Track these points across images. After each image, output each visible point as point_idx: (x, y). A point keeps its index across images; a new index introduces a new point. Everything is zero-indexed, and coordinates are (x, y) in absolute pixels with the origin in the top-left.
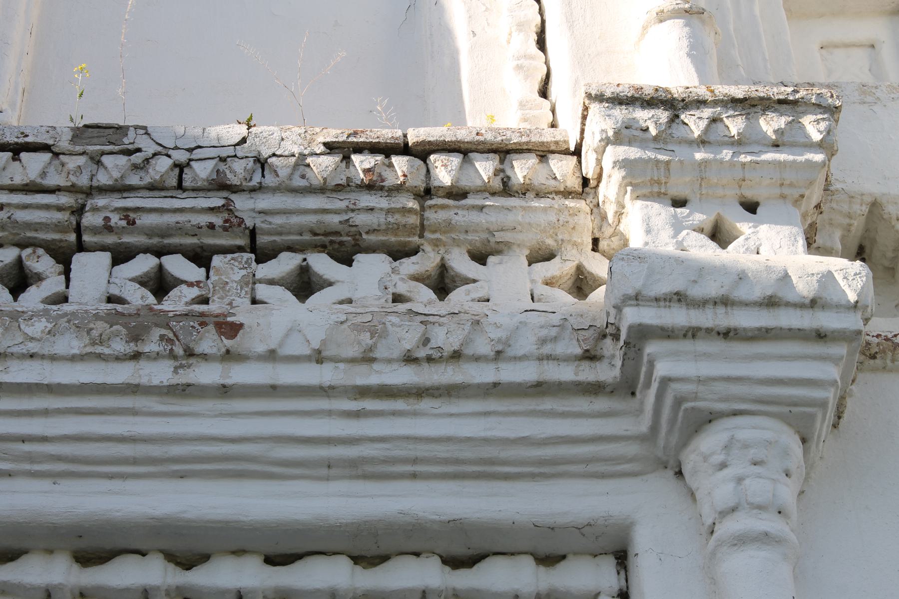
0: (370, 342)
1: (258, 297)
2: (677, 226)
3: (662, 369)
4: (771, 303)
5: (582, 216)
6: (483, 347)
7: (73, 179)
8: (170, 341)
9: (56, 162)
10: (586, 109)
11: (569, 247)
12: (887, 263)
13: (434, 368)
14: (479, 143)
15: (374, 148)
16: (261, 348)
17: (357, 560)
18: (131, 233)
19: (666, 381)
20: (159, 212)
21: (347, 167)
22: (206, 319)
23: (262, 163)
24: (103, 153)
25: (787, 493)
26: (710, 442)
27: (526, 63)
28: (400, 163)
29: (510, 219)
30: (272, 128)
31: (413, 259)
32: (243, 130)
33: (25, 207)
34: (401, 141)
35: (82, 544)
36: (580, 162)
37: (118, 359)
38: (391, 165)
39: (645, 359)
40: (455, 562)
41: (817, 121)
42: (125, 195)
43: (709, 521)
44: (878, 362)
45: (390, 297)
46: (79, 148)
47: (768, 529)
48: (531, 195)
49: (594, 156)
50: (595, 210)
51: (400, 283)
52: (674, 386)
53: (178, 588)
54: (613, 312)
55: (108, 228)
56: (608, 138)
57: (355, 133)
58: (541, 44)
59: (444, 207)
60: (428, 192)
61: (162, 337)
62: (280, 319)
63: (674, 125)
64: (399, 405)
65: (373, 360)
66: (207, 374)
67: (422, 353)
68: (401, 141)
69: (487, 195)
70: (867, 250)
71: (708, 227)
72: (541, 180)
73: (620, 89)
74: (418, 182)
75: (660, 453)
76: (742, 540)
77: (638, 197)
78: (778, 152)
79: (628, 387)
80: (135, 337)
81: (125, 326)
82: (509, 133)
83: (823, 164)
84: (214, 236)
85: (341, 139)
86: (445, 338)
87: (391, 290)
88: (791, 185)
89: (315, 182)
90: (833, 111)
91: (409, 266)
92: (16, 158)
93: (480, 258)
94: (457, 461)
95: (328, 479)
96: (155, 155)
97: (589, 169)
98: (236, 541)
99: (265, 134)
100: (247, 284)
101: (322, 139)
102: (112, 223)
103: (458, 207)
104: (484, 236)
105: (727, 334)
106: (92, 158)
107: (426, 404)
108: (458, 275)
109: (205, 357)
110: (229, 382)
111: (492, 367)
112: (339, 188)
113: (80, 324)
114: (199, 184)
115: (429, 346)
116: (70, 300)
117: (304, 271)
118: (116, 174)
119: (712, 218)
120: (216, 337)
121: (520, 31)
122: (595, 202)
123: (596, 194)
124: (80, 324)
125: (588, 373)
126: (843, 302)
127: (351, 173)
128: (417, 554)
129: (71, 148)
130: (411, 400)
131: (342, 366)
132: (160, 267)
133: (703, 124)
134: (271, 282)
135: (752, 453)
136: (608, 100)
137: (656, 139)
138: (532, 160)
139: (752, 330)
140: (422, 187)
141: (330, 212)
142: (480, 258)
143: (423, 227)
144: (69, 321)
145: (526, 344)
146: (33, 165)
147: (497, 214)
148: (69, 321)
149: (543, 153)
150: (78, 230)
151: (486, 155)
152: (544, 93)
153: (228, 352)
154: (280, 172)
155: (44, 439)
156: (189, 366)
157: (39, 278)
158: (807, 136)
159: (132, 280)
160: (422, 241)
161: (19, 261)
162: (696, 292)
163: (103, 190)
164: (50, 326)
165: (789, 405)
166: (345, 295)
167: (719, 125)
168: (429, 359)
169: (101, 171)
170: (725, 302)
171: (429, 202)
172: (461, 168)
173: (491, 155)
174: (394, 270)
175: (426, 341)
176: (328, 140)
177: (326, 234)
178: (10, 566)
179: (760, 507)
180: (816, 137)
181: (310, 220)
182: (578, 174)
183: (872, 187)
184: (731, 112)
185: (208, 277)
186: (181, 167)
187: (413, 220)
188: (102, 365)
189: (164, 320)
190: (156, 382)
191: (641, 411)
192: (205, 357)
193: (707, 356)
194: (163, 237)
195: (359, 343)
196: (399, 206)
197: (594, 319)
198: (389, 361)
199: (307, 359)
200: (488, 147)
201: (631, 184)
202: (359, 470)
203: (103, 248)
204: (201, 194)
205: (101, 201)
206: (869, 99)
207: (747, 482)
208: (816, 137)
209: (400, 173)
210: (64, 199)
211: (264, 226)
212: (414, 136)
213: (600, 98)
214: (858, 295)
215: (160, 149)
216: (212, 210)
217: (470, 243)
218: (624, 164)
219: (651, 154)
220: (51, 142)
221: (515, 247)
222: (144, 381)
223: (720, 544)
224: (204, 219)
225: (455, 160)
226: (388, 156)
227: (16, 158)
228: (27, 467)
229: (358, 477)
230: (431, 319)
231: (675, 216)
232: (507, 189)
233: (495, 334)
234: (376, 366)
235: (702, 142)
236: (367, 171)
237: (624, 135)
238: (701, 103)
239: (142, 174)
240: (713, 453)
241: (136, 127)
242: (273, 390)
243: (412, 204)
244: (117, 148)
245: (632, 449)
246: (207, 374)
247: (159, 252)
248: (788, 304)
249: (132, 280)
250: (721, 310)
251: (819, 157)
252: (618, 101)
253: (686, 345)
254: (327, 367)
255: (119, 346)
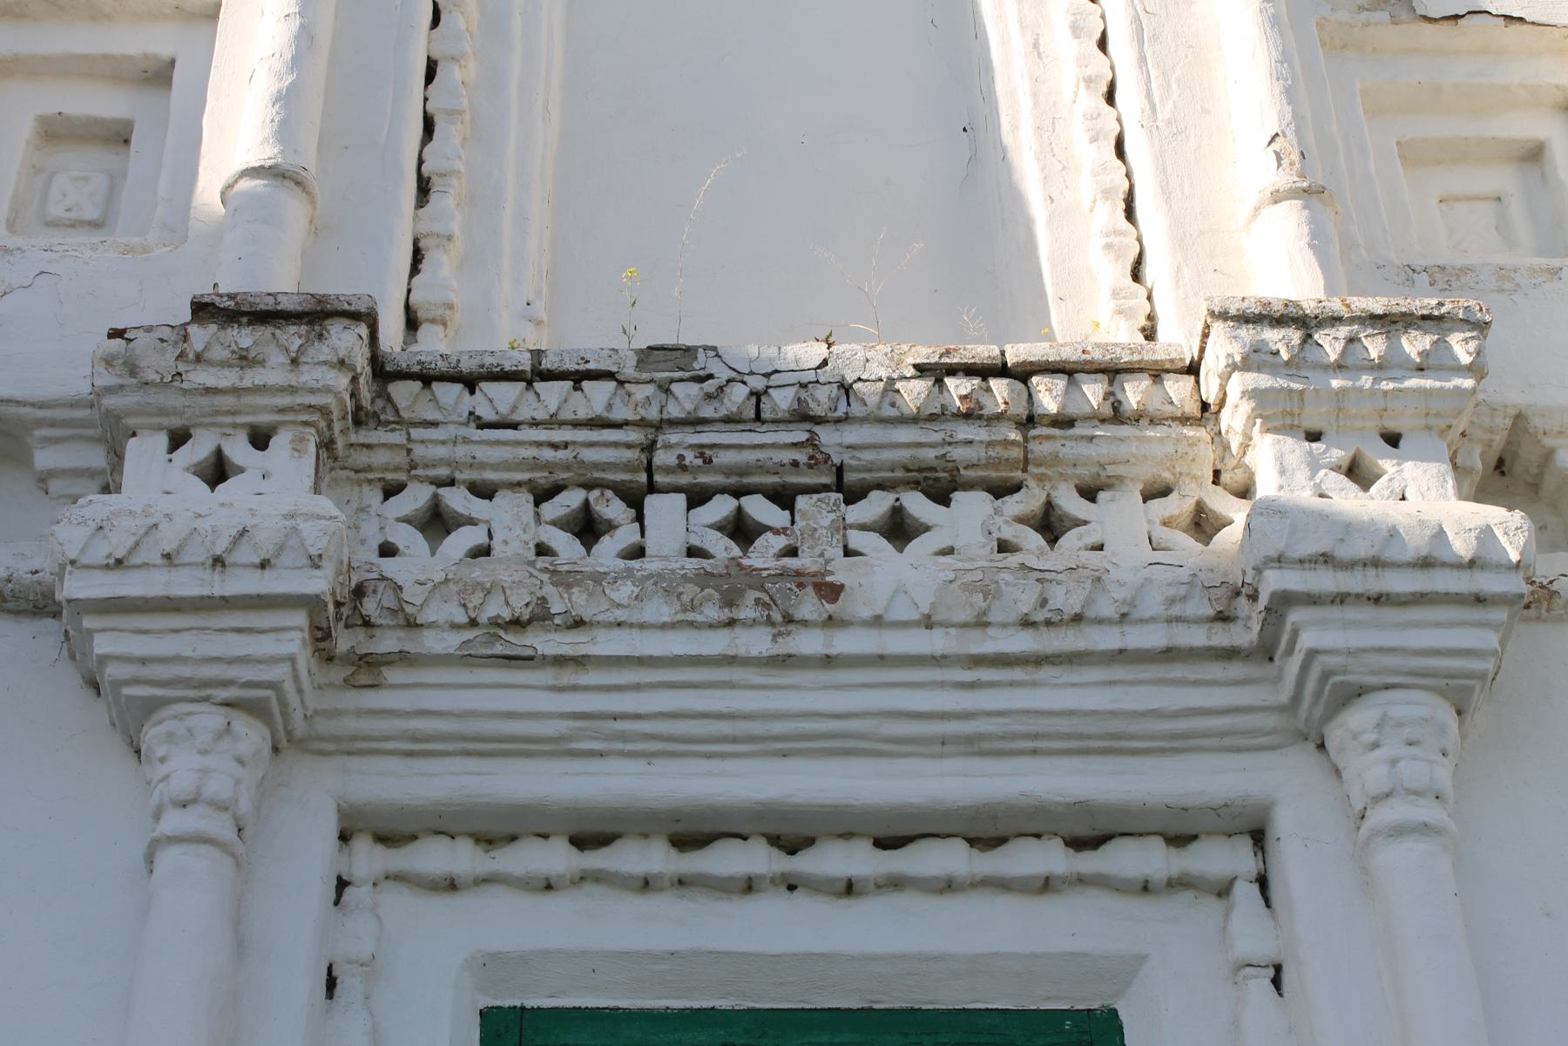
0: (984, 605)
1: (851, 546)
2: (1314, 466)
3: (1307, 640)
4: (1425, 563)
5: (1202, 446)
6: (1106, 609)
7: (642, 412)
8: (765, 605)
9: (621, 392)
10: (1207, 327)
11: (1187, 480)
12: (1529, 479)
13: (1053, 632)
14: (1086, 362)
15: (970, 370)
16: (866, 613)
17: (972, 842)
18: (707, 472)
19: (1312, 654)
20: (740, 448)
21: (941, 392)
22: (802, 579)
23: (846, 388)
24: (672, 381)
25: (1443, 775)
26: (1360, 718)
27: (1116, 240)
28: (999, 386)
29: (1122, 451)
30: (854, 346)
31: (1016, 496)
32: (816, 352)
33: (592, 445)
34: (999, 361)
35: (680, 828)
36: (1198, 382)
37: (711, 626)
38: (989, 390)
39: (1288, 627)
40: (1078, 844)
41: (1466, 340)
42: (699, 428)
43: (1360, 806)
44: (1532, 612)
45: (995, 544)
46: (646, 376)
47: (1426, 819)
48: (1144, 422)
49: (1218, 381)
50: (1217, 439)
51: (1005, 528)
52: (1321, 658)
53: (783, 874)
54: (1250, 572)
55: (682, 467)
56: (1234, 364)
57: (948, 352)
58: (1130, 213)
59: (1049, 437)
60: (1030, 421)
61: (757, 601)
62: (885, 577)
63: (1307, 346)
64: (1017, 674)
65: (987, 625)
66: (808, 643)
67: (1040, 616)
68: (999, 361)
69: (1096, 422)
70: (1508, 463)
71: (1345, 464)
72: (1155, 405)
73: (1246, 304)
74: (1021, 410)
75: (1300, 725)
76: (1399, 831)
77: (1268, 431)
78: (1422, 377)
79: (1266, 651)
80: (730, 601)
81: (717, 588)
82: (1118, 350)
83: (1474, 391)
84: (798, 474)
85: (933, 360)
86: (1065, 599)
87: (996, 535)
88: (1438, 415)
89: (906, 412)
90: (1482, 327)
91: (1014, 505)
92: (577, 387)
93: (1089, 493)
94: (1082, 737)
95: (941, 756)
96: (729, 381)
97: (1210, 392)
98: (845, 825)
99: (848, 354)
100: (838, 530)
101: (911, 360)
102: (687, 462)
103: (1065, 438)
104: (1095, 469)
105: (1377, 599)
106: (660, 387)
107: (1046, 673)
108: (1066, 515)
109: (805, 623)
110: (833, 651)
111: (1116, 630)
112: (933, 418)
113: (667, 585)
114: (780, 415)
115: (1048, 607)
116: (648, 552)
117: (897, 512)
118: (689, 406)
119: (1351, 454)
120: (816, 600)
121: (1107, 199)
122: (1216, 429)
123: (1217, 421)
124: (667, 585)
125: (1222, 637)
126: (1504, 562)
127: (944, 399)
128: (1038, 836)
129: (637, 375)
130: (1030, 669)
131: (953, 631)
132: (740, 509)
133: (1339, 346)
134: (863, 527)
135: (1407, 732)
136: (1233, 318)
137: (1287, 363)
138: (1145, 382)
139: (1405, 595)
140: (1024, 414)
141: (922, 445)
142: (1089, 493)
143: (1026, 458)
144: (655, 584)
145: (1152, 605)
146: (598, 395)
147: (1107, 445)
148: (655, 584)
149: (1157, 373)
150: (649, 469)
151: (1093, 376)
152: (1136, 275)
153: (830, 617)
154: (868, 401)
155: (637, 717)
156: (789, 634)
157: (611, 527)
158: (1455, 358)
159: (711, 526)
160: (1026, 476)
161: (587, 504)
162: (1344, 552)
163: (674, 423)
164: (637, 590)
165: (1447, 677)
166: (945, 543)
167: (1357, 345)
168: (1048, 623)
169: (671, 401)
170: (1376, 563)
171: (1033, 433)
172: (1067, 391)
173: (1100, 376)
174: (997, 511)
175: (1044, 602)
176: (918, 361)
177: (920, 470)
178: (604, 851)
179: (1417, 793)
180: (1466, 359)
181: (903, 455)
182: (1196, 397)
183: (1517, 397)
184: (1370, 331)
185: (793, 522)
186: (757, 395)
187: (1016, 453)
188: (694, 633)
189: (756, 579)
190: (754, 653)
191: (1278, 679)
192: (805, 623)
193: (1357, 624)
194: (741, 475)
195: (972, 606)
196: (1001, 438)
197: (1226, 575)
198: (1005, 625)
199: (917, 624)
200: (1096, 366)
201: (1261, 416)
202: (973, 746)
203: (677, 489)
204: (782, 427)
205: (673, 437)
206: (1508, 286)
207: (1402, 764)
208: (1466, 359)
209: (1000, 400)
210: (634, 436)
211: (853, 462)
212: (1015, 354)
213: (1224, 316)
214: (1521, 554)
215: (734, 374)
216: (795, 445)
217: (1079, 477)
218: (1254, 394)
219: (1282, 382)
220: (614, 369)
221: (1128, 482)
222: (742, 651)
223: (1375, 833)
224: (787, 456)
225: (1060, 383)
226: (985, 379)
227: (577, 387)
228: (620, 746)
229: (974, 754)
230: (1047, 576)
231: (1310, 453)
232: (1117, 415)
233: (1120, 594)
234: (990, 631)
235: (1339, 367)
236: (963, 398)
237: (1256, 359)
238: (1336, 320)
239: (716, 404)
240: (1362, 732)
241: (706, 348)
242: (880, 660)
243: (1014, 435)
244: (687, 374)
245: (1271, 721)
246: (808, 643)
247: (738, 493)
248: (1444, 565)
249: (711, 526)
250: (1371, 572)
251: (1468, 383)
252: (1245, 319)
253: (1334, 612)
254: (938, 633)
255: (712, 612)
